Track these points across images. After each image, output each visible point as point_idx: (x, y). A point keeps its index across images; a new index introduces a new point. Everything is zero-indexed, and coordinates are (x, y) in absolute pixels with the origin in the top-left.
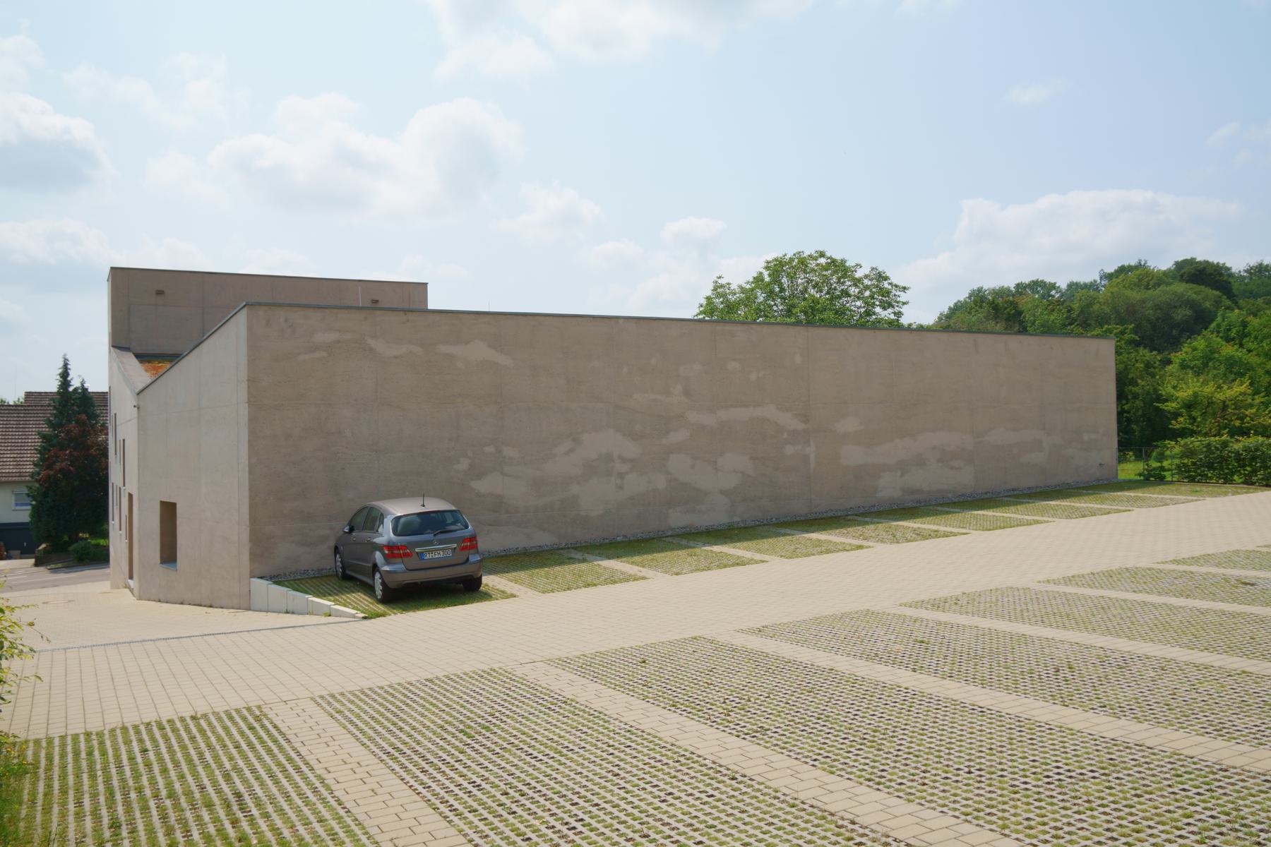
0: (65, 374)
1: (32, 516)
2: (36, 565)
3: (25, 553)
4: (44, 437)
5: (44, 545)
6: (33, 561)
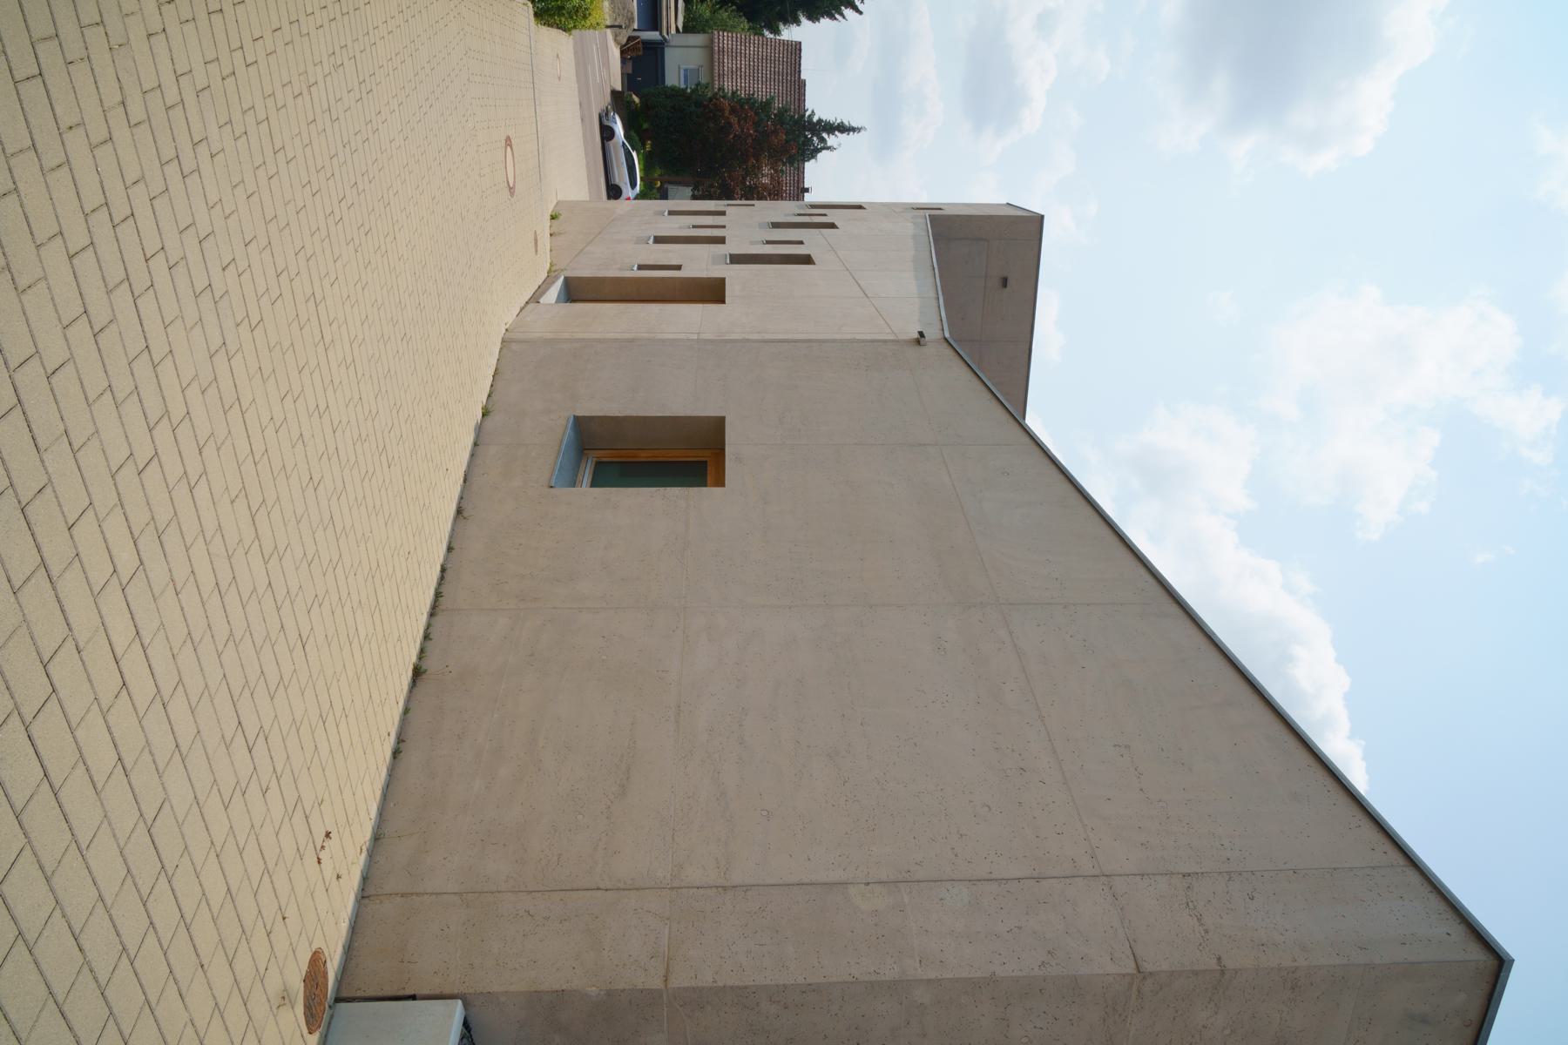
0: (843, 128)
1: (673, 89)
2: (614, 93)
3: (628, 79)
4: (767, 105)
5: (637, 100)
6: (619, 88)
